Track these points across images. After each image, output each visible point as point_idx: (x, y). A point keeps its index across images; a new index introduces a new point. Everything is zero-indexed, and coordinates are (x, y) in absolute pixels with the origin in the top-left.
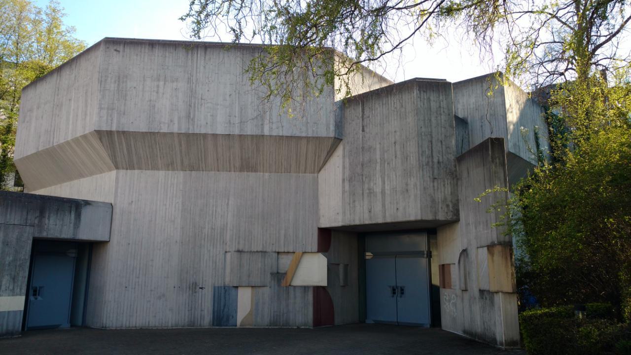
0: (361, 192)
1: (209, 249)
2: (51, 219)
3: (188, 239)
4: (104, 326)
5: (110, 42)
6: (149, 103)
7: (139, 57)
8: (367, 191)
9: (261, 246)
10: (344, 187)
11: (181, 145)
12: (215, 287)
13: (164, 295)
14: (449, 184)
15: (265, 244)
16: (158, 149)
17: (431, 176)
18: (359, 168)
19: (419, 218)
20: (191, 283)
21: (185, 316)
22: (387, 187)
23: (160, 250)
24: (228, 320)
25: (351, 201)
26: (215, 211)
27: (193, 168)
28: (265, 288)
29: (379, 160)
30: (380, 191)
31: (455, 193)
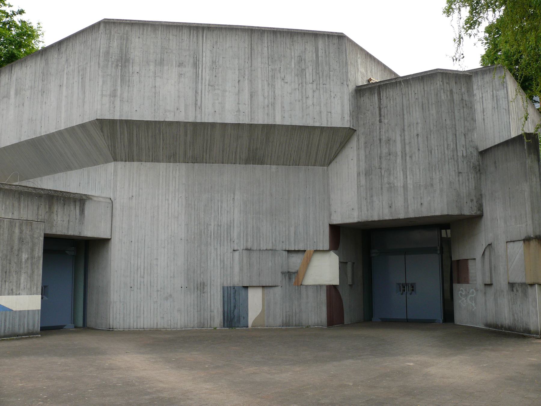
0: (380, 186)
1: (216, 247)
2: (59, 214)
3: (193, 237)
4: (112, 327)
5: (107, 23)
6: (153, 90)
7: (141, 39)
8: (387, 186)
9: (271, 245)
10: (359, 181)
11: (186, 135)
12: (223, 288)
13: (171, 296)
14: (473, 178)
15: (274, 242)
16: (162, 140)
17: (456, 170)
18: (377, 161)
19: (445, 213)
20: (199, 283)
21: (194, 316)
22: (409, 181)
23: (164, 247)
24: (239, 321)
25: (368, 195)
26: (221, 206)
27: (196, 160)
28: (277, 288)
29: (399, 153)
30: (402, 185)
31: (478, 188)
